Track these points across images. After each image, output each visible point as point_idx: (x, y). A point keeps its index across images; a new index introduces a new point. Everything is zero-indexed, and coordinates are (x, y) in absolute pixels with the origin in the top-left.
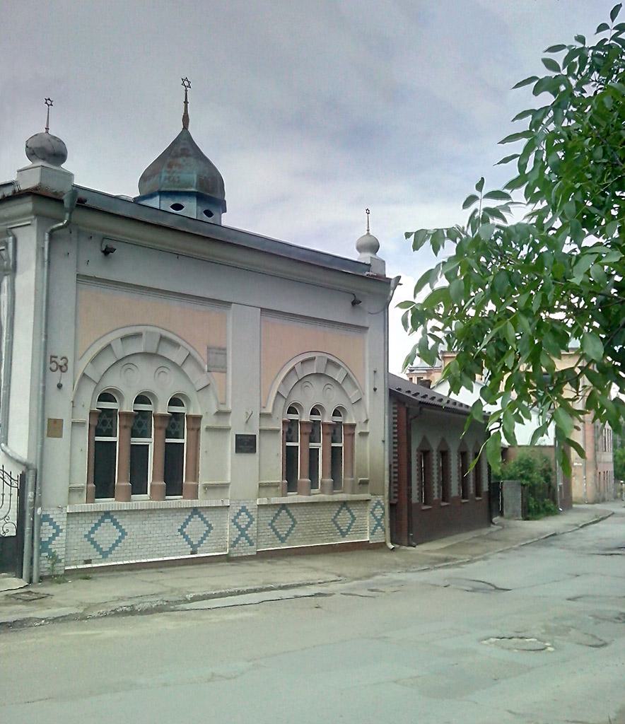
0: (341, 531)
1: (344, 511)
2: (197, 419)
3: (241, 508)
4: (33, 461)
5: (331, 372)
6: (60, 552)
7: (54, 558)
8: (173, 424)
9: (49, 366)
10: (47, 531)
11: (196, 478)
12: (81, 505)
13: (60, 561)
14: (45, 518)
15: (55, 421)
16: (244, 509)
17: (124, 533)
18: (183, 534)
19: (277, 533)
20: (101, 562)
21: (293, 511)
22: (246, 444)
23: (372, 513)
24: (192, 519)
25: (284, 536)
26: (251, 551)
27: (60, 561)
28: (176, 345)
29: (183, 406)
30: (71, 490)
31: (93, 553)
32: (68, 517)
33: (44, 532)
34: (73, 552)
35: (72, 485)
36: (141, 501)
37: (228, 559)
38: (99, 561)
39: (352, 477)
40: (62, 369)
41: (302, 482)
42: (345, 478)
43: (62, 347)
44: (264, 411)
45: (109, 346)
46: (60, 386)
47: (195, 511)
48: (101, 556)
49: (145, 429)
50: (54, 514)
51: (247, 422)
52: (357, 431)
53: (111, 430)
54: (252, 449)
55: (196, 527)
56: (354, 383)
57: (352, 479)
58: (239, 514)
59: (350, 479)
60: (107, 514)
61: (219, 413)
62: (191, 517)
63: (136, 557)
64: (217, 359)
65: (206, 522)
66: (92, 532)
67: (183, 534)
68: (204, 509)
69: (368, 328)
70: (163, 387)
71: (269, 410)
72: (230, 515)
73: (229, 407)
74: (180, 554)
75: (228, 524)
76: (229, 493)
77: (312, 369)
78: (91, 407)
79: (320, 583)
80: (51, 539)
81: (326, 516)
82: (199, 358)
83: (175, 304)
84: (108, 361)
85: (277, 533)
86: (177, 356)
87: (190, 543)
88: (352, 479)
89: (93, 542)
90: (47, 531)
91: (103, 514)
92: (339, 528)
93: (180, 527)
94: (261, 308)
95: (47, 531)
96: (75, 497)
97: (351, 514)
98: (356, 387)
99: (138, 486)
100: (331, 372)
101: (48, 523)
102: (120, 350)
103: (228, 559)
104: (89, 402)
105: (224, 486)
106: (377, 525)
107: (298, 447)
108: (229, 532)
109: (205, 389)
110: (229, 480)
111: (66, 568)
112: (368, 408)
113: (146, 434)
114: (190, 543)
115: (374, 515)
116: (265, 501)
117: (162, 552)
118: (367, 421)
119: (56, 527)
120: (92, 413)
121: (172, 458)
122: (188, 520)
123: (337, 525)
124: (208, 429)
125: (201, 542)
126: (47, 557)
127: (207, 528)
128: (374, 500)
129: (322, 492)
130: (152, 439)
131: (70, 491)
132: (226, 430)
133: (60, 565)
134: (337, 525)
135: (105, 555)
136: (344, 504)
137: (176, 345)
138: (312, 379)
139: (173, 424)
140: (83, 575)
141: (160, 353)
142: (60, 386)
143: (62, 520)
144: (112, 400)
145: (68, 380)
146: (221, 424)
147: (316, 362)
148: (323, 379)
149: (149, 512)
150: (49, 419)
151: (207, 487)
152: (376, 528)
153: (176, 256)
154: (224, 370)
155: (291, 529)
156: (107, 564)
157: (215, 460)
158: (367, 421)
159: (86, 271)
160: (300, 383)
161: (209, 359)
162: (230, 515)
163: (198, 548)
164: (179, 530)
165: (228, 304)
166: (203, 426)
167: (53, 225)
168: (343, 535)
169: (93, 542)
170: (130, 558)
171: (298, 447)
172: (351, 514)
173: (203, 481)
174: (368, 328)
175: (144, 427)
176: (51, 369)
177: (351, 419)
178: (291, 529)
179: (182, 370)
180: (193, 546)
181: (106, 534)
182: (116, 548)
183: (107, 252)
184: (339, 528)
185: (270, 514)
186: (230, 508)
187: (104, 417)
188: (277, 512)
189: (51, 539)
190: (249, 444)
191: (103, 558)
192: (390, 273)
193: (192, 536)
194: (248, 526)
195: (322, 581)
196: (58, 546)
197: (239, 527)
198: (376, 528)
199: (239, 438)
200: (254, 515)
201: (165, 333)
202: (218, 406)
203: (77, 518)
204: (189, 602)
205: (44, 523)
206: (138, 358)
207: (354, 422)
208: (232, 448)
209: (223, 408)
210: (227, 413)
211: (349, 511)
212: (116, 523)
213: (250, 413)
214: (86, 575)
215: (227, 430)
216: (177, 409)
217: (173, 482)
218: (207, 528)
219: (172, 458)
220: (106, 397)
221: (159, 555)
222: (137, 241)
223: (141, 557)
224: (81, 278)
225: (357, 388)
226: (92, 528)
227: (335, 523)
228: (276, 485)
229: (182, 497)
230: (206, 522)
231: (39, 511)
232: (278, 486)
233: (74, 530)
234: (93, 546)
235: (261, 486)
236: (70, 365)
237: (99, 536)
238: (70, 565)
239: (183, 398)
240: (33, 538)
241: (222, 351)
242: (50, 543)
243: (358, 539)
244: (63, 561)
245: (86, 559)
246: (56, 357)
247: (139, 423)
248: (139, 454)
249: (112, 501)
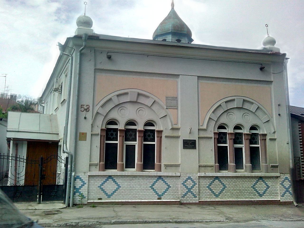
0: (259, 193)
1: (261, 182)
2: (160, 132)
3: (187, 177)
4: (73, 152)
5: (246, 106)
6: (85, 194)
7: (83, 196)
8: (148, 135)
9: (80, 109)
10: (78, 184)
11: (160, 161)
12: (96, 172)
13: (85, 198)
14: (78, 177)
15: (83, 134)
16: (189, 178)
17: (119, 186)
18: (153, 189)
19: (213, 192)
20: (107, 200)
21: (224, 181)
22: (189, 144)
23: (282, 184)
24: (158, 182)
25: (218, 194)
26: (196, 200)
27: (85, 198)
28: (147, 97)
29: (258, 130)
30: (90, 165)
31: (102, 195)
32: (89, 177)
33: (77, 183)
34: (92, 194)
35: (91, 163)
36: (130, 171)
37: (180, 204)
38: (106, 199)
39: (266, 163)
40: (87, 110)
41: (230, 165)
42: (262, 163)
43: (87, 100)
44: (201, 128)
45: (220, 105)
46: (85, 118)
47: (160, 177)
48: (107, 197)
49: (256, 141)
50: (81, 175)
51: (190, 133)
52: (268, 138)
53: (241, 142)
54: (193, 147)
55: (160, 186)
56: (264, 112)
57: (266, 164)
58: (186, 181)
59: (264, 164)
60: (110, 177)
61: (173, 129)
62: (157, 181)
63: (126, 199)
64: (172, 103)
65: (166, 184)
66: (102, 184)
67: (153, 189)
68: (165, 177)
69: (272, 81)
70: (247, 122)
71: (205, 127)
72: (181, 181)
73: (179, 126)
74: (151, 199)
75: (180, 185)
76: (180, 169)
77: (234, 105)
78: (101, 127)
79: (207, 222)
80: (81, 187)
81: (248, 184)
82: (161, 103)
83: (147, 78)
84: (110, 106)
85: (213, 192)
86: (149, 102)
87: (157, 194)
88: (266, 164)
89: (102, 190)
90: (78, 183)
91: (108, 177)
92: (257, 192)
93: (99, 185)
94: (198, 76)
95: (78, 183)
96: (93, 168)
97: (266, 184)
98: (265, 114)
99: (130, 163)
100: (246, 106)
101: (79, 180)
102: (116, 101)
103: (180, 204)
104: (100, 124)
105: (177, 166)
106: (286, 192)
107: (118, 143)
108: (182, 190)
109: (164, 118)
110: (180, 163)
111: (88, 201)
112: (275, 124)
113: (241, 143)
114: (157, 194)
115: (283, 185)
116: (203, 174)
117: (141, 197)
118: (274, 132)
119: (83, 182)
120: (102, 130)
121: (254, 154)
122: (155, 182)
123: (256, 190)
124: (166, 137)
125: (163, 194)
126: (78, 195)
127: (167, 187)
128: (283, 177)
129: (246, 171)
130: (244, 145)
131: (90, 165)
132: (178, 137)
133: (85, 199)
134: (256, 190)
135: (109, 196)
136: (261, 178)
137: (147, 97)
138: (235, 111)
139: (148, 135)
140: (92, 205)
141: (138, 101)
142: (85, 118)
143: (86, 178)
144: (224, 128)
145: (89, 115)
146: (175, 134)
147: (235, 102)
148: (242, 110)
149: (133, 177)
150: (80, 133)
151: (166, 166)
152: (285, 193)
153: (147, 56)
154: (176, 108)
155: (222, 191)
156: (110, 201)
157: (170, 152)
158: (274, 132)
159: (99, 67)
160: (226, 114)
161: (167, 103)
162: (181, 181)
163: (162, 197)
164: (120, 187)
165: (179, 75)
166: (164, 135)
167: (80, 49)
168: (261, 196)
169: (102, 190)
170: (122, 199)
171: (118, 143)
172: (266, 184)
173: (164, 162)
174: (272, 81)
175: (240, 140)
176: (81, 110)
177: (263, 131)
178: (222, 191)
179: (152, 109)
180: (158, 195)
181: (110, 186)
182: (115, 193)
183: (109, 58)
184: (257, 192)
185: (207, 182)
186: (181, 177)
187: (222, 135)
188: (105, 180)
189: (81, 187)
190: (191, 144)
191: (108, 198)
192: (282, 52)
193: (158, 190)
194: (192, 187)
195: (208, 221)
196: (84, 191)
197: (187, 187)
198: (285, 193)
199: (185, 141)
200: (197, 182)
201: (140, 92)
202: (172, 125)
203: (94, 178)
204: (112, 224)
205: (77, 180)
206: (128, 104)
207: (266, 133)
208: (181, 147)
209: (175, 126)
210: (178, 129)
211: (265, 183)
212: (115, 181)
213: (190, 128)
214: (94, 205)
215: (178, 137)
216: (255, 132)
217: (149, 161)
218: (167, 187)
219: (254, 154)
220: (222, 127)
221: (139, 199)
222: (123, 51)
223: (129, 199)
224: (96, 70)
225: (266, 114)
226: (102, 183)
227: (254, 188)
228: (212, 166)
229: (228, 171)
230: (166, 184)
231: (73, 174)
232: (97, 165)
233: (93, 183)
234: (102, 192)
235: (200, 166)
236: (91, 108)
237: (106, 187)
238: (91, 200)
239: (257, 127)
240: (70, 186)
241: (175, 99)
242: (80, 189)
243: (272, 198)
244: (86, 198)
245: (99, 198)
246: (84, 105)
247: (129, 134)
248: (130, 150)
249: (116, 171)
